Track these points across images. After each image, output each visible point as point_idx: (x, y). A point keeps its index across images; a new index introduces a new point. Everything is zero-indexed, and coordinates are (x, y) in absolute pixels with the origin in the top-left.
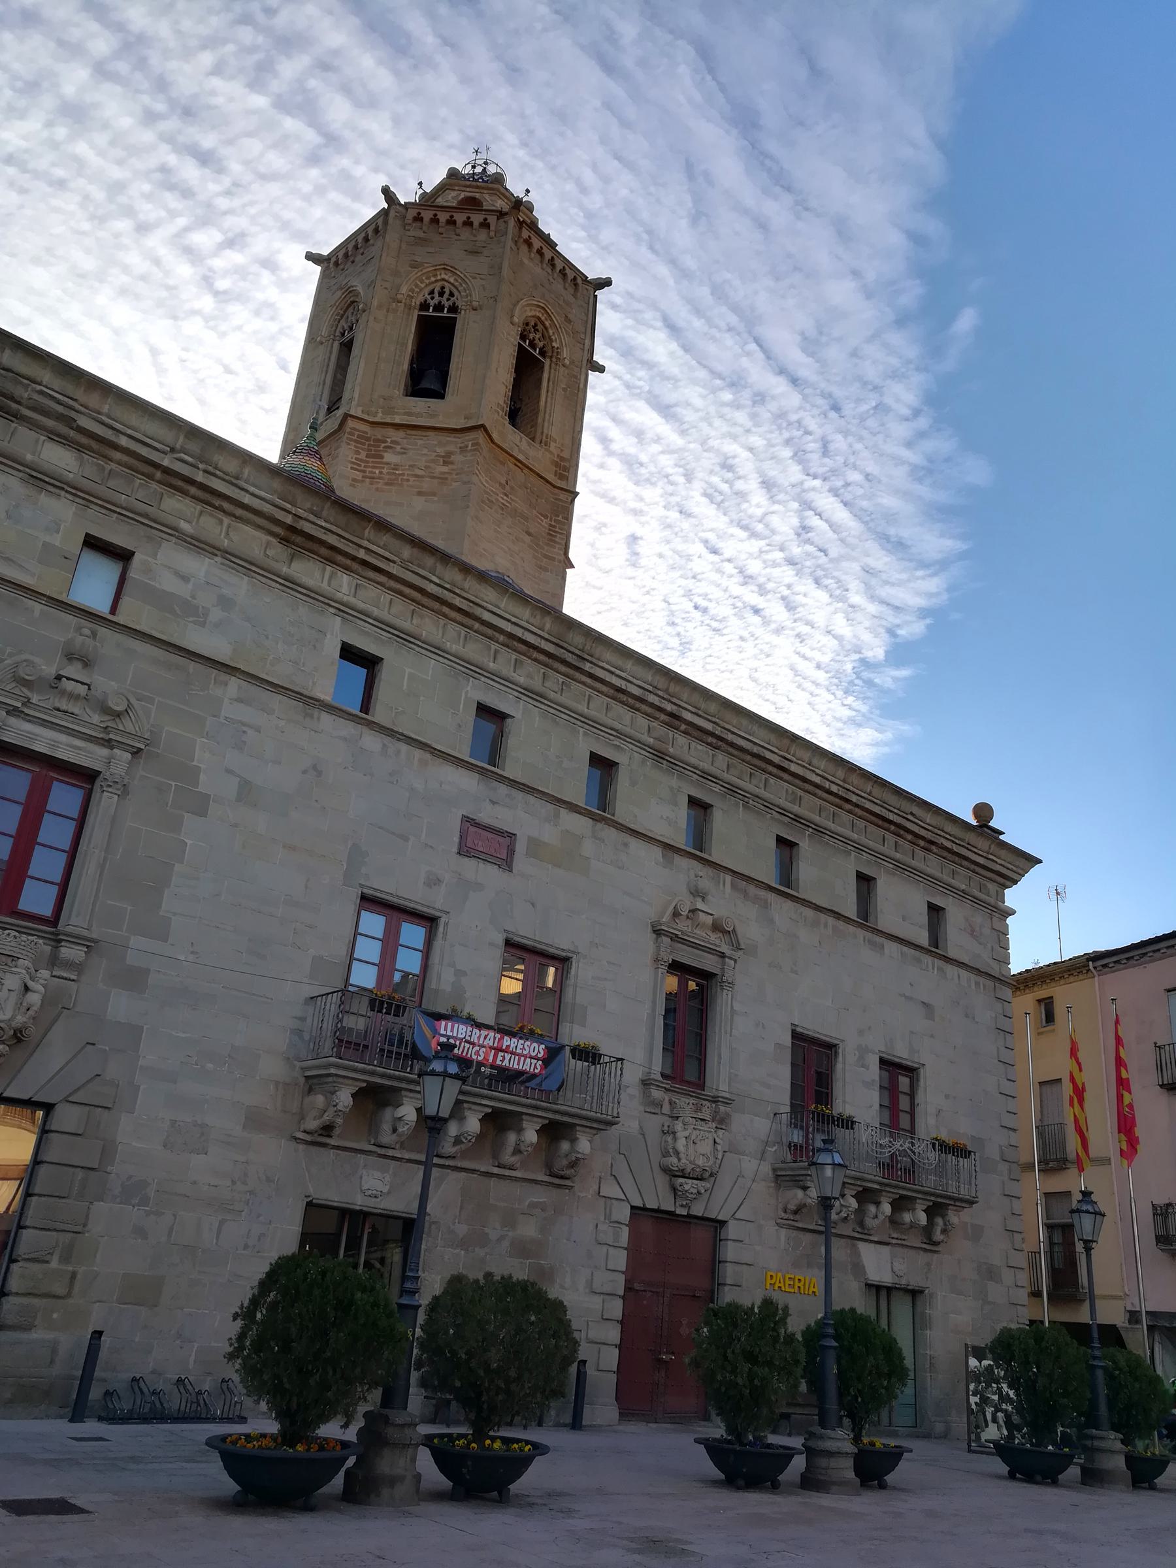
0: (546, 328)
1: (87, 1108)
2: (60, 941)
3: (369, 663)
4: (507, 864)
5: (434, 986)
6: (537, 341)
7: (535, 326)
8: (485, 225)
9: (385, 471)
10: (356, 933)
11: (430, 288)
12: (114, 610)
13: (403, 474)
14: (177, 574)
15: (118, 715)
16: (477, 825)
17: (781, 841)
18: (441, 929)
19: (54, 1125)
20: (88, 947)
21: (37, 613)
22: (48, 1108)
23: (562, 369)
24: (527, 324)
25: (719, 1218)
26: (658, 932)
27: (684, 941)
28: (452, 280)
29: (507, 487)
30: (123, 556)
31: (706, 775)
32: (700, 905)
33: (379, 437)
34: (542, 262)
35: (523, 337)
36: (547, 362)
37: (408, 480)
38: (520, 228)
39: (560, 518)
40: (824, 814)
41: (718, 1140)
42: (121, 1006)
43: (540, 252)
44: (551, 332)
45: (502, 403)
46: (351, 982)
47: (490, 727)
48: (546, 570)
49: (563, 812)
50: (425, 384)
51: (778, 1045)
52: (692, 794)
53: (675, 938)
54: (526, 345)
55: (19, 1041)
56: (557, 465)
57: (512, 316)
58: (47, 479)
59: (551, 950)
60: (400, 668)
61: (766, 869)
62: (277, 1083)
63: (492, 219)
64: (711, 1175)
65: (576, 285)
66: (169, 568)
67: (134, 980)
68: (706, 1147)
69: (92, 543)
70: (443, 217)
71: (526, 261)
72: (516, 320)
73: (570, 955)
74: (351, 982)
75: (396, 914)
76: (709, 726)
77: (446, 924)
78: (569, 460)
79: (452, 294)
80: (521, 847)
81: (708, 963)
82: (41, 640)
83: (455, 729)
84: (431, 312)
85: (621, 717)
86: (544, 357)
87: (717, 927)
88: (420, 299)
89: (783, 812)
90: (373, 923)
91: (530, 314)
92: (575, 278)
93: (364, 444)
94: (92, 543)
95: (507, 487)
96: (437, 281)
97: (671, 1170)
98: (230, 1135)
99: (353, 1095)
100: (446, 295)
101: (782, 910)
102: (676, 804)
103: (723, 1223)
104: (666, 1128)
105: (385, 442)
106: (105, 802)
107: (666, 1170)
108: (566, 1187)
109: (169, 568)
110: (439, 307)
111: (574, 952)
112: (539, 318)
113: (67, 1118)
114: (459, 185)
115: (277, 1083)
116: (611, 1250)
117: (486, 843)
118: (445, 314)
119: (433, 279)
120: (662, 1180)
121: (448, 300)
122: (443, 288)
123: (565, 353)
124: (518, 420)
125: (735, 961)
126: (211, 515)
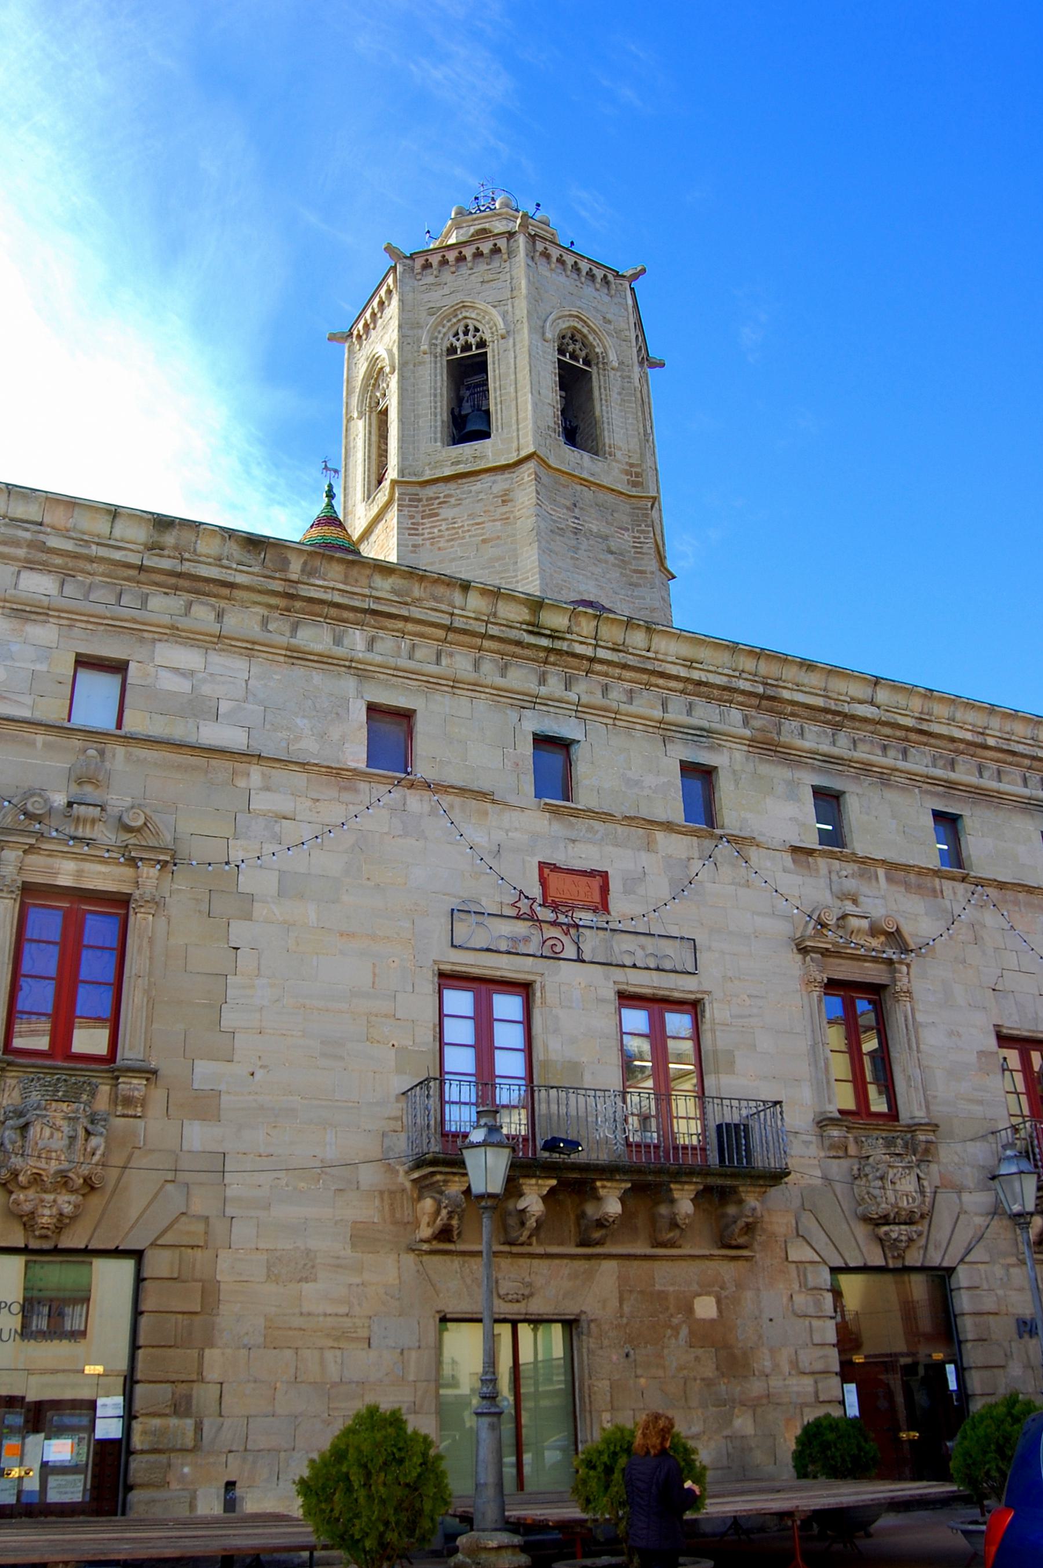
0: (585, 336)
1: (177, 1251)
2: (117, 1078)
3: (563, 745)
5: (541, 1057)
6: (578, 352)
7: (572, 338)
8: (496, 250)
9: (443, 528)
10: (441, 1015)
11: (454, 330)
12: (119, 725)
13: (463, 526)
14: (176, 670)
15: (138, 830)
16: (555, 868)
17: (938, 815)
18: (538, 994)
19: (146, 1273)
20: (148, 1079)
21: (39, 745)
22: (137, 1255)
23: (612, 373)
24: (563, 337)
25: (945, 1264)
26: (804, 951)
27: (838, 954)
28: (473, 316)
29: (576, 510)
30: (118, 668)
31: (830, 759)
32: (849, 907)
33: (432, 495)
34: (565, 270)
35: (561, 351)
36: (593, 370)
37: (469, 531)
38: (534, 243)
39: (643, 527)
40: (986, 774)
41: (922, 1175)
42: (198, 1136)
43: (560, 261)
44: (591, 338)
45: (552, 425)
46: (447, 1069)
47: (556, 759)
48: (637, 585)
49: (660, 836)
50: (471, 427)
51: (981, 1053)
52: (816, 783)
53: (825, 953)
54: (567, 359)
55: (93, 1188)
56: (628, 473)
57: (543, 334)
58: (674, 728)
59: (676, 995)
60: (433, 716)
61: (928, 850)
62: (381, 1193)
63: (502, 243)
64: (922, 1216)
65: (608, 283)
66: (168, 669)
67: (206, 1106)
68: (908, 1185)
69: (83, 662)
70: (451, 256)
71: (548, 274)
72: (549, 335)
73: (699, 996)
74: (447, 1069)
75: (484, 987)
76: (819, 702)
77: (543, 987)
78: (640, 465)
79: (477, 330)
80: (615, 885)
81: (872, 973)
82: (44, 771)
83: (511, 768)
84: (459, 355)
85: (705, 714)
86: (590, 366)
87: (875, 931)
88: (446, 344)
89: (934, 781)
90: (460, 1001)
91: (564, 326)
92: (605, 276)
93: (417, 507)
94: (83, 662)
95: (576, 510)
96: (459, 321)
97: (871, 1219)
98: (338, 1258)
99: (692, 1200)
100: (471, 333)
101: (954, 893)
102: (799, 800)
103: (951, 1270)
104: (855, 1172)
105: (438, 498)
106: (140, 921)
107: (866, 1219)
108: (747, 1259)
109: (168, 669)
110: (467, 347)
111: (705, 992)
112: (575, 328)
113: (158, 1264)
114: (467, 221)
115: (381, 1193)
116: (816, 1323)
118: (474, 351)
119: (455, 320)
120: (861, 1231)
121: (474, 336)
122: (467, 326)
123: (612, 357)
124: (578, 439)
125: (908, 966)
126: (202, 603)
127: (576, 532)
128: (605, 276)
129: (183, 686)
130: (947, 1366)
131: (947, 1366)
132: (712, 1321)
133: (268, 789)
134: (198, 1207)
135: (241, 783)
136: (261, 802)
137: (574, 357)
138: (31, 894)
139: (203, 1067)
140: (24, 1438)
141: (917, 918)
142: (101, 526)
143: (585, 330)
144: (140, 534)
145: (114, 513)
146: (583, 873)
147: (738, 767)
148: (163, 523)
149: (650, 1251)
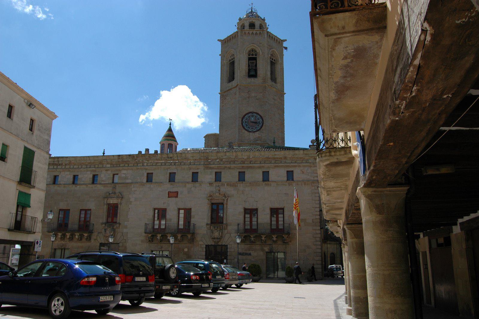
4: (177, 197)
16: (170, 192)
24: (250, 51)
35: (249, 55)
42: (125, 230)
49: (187, 185)
67: (126, 227)
80: (179, 193)
88: (229, 59)
92: (260, 32)
110: (232, 59)
117: (173, 195)
127: (249, 97)
128: (260, 32)
129: (124, 175)
130: (225, 260)
131: (225, 260)
132: (186, 252)
133: (134, 187)
134: (125, 238)
135: (131, 187)
136: (133, 189)
137: (253, 55)
138: (109, 205)
139: (126, 223)
140: (320, 245)
141: (231, 191)
142: (113, 158)
143: (255, 48)
144: (117, 158)
145: (113, 156)
146: (174, 192)
147: (202, 171)
148: (119, 156)
149: (178, 243)
